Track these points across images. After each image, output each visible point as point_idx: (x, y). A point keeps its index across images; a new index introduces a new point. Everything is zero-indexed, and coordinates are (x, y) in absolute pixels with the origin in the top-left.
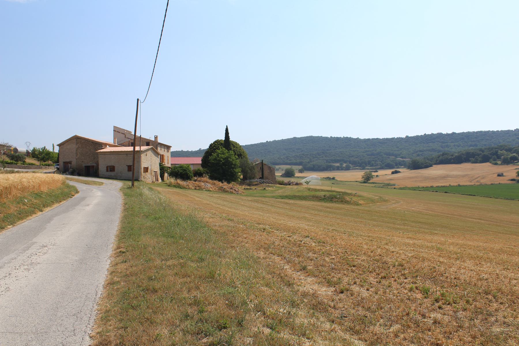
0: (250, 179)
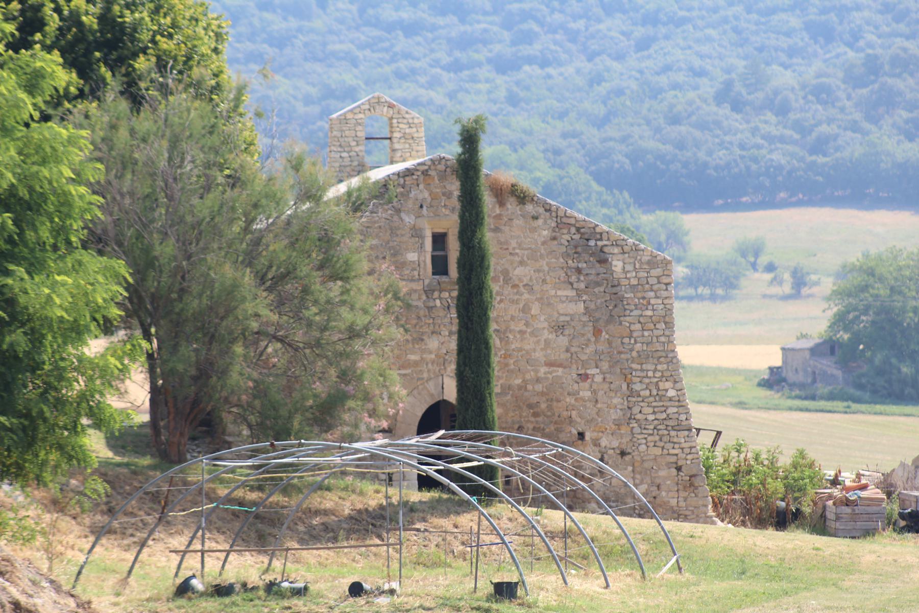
0: (273, 427)
